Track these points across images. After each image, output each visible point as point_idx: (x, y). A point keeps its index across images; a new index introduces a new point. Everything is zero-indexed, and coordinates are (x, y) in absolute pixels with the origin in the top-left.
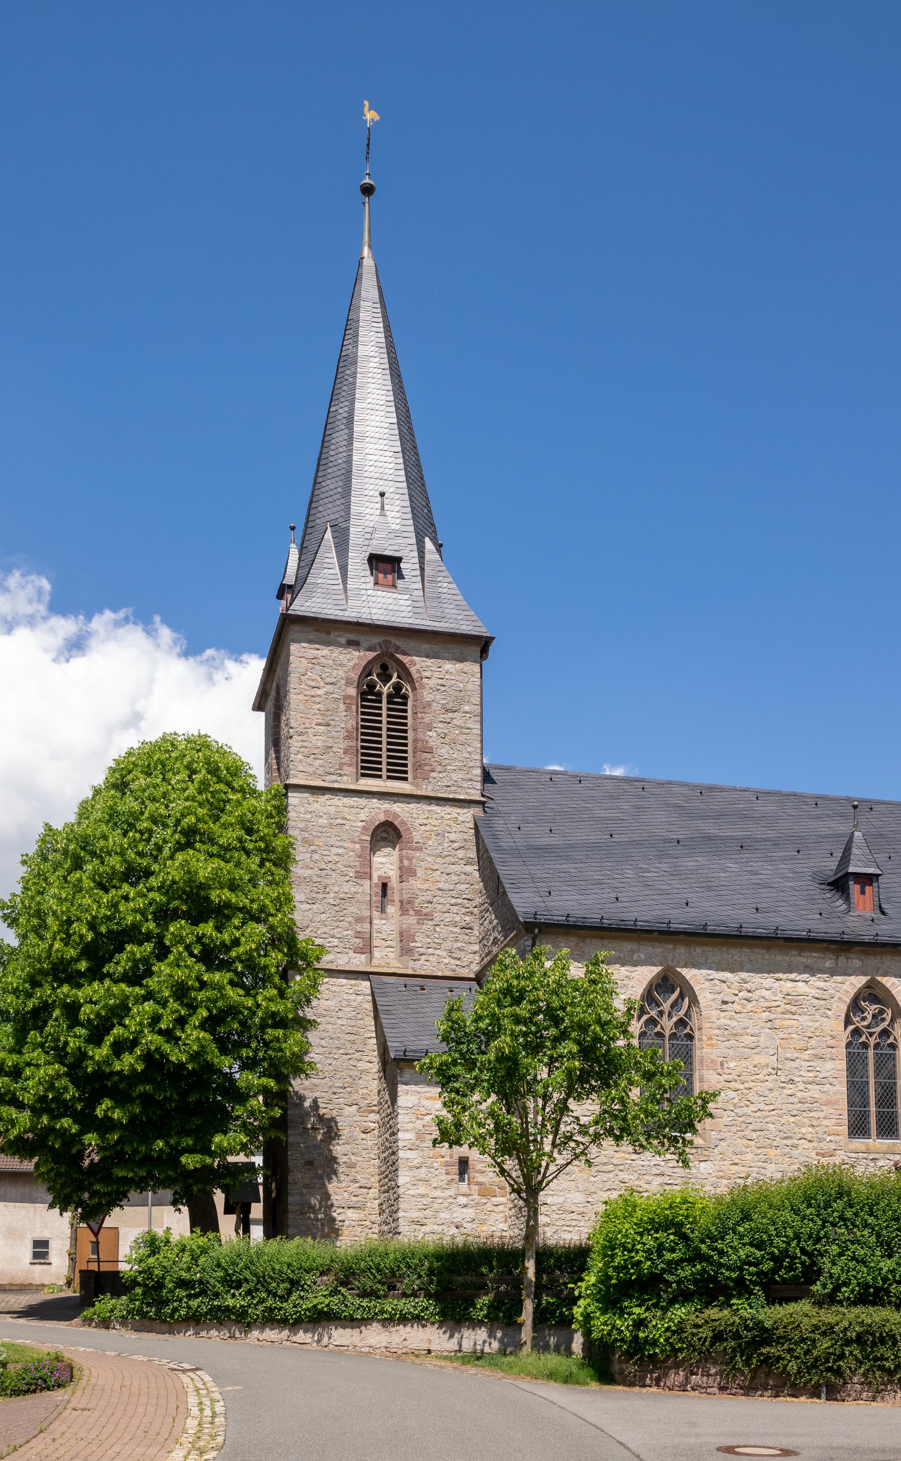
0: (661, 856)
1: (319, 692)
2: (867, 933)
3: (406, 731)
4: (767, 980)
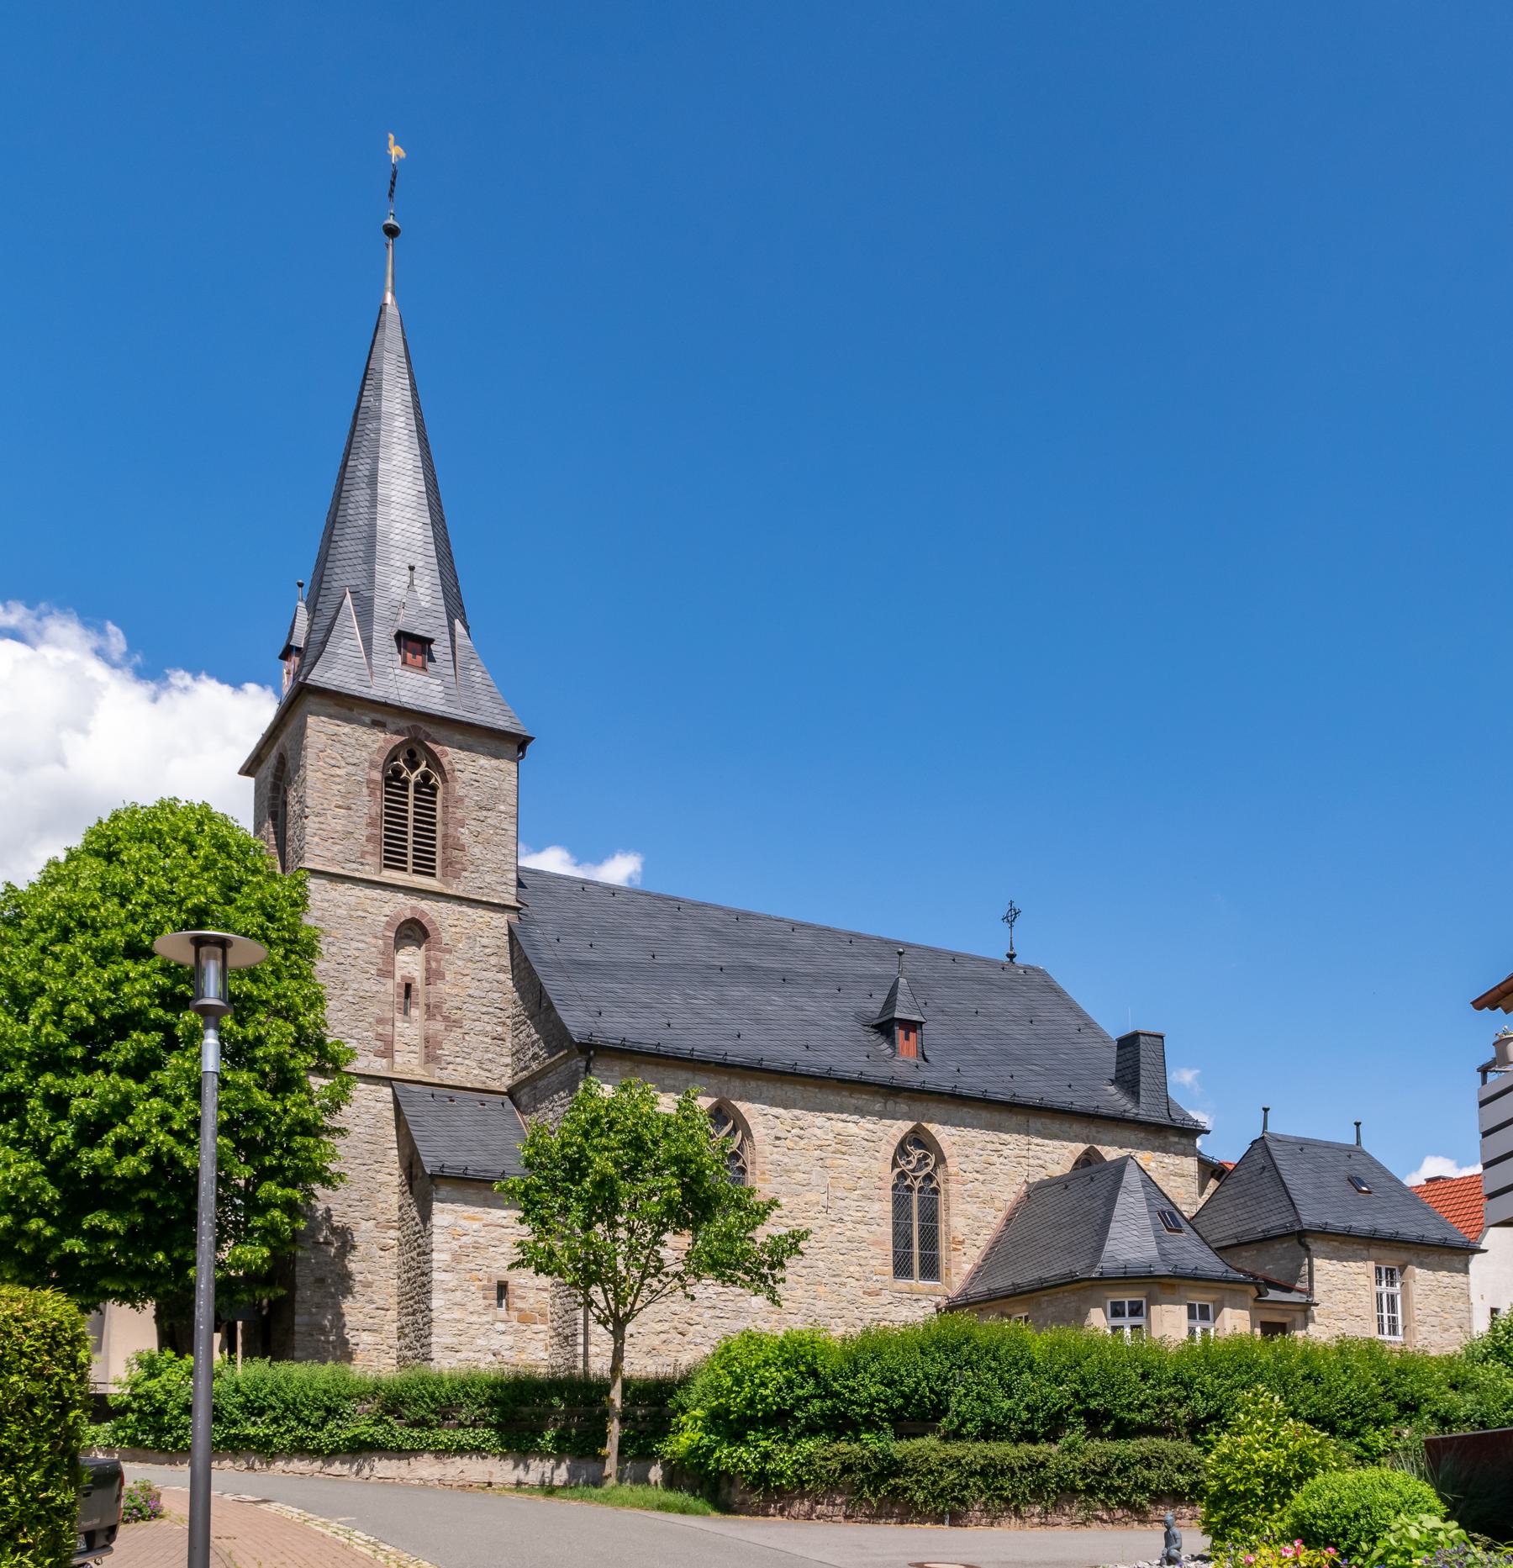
0: (707, 983)
1: (339, 772)
2: (915, 1079)
3: (434, 824)
4: (819, 1119)
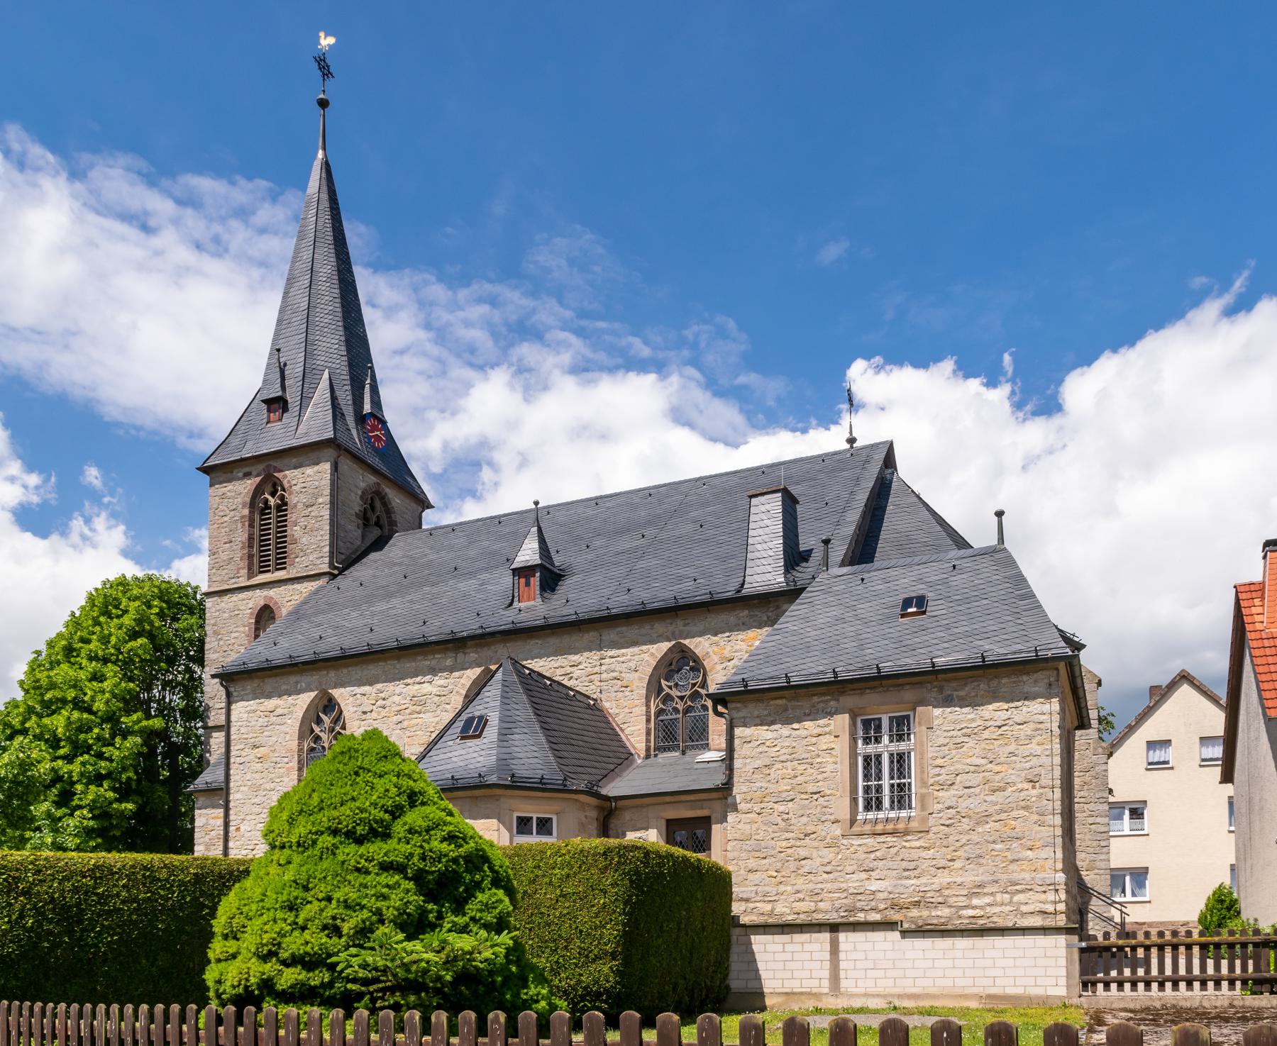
1: (225, 519)
4: (398, 687)
